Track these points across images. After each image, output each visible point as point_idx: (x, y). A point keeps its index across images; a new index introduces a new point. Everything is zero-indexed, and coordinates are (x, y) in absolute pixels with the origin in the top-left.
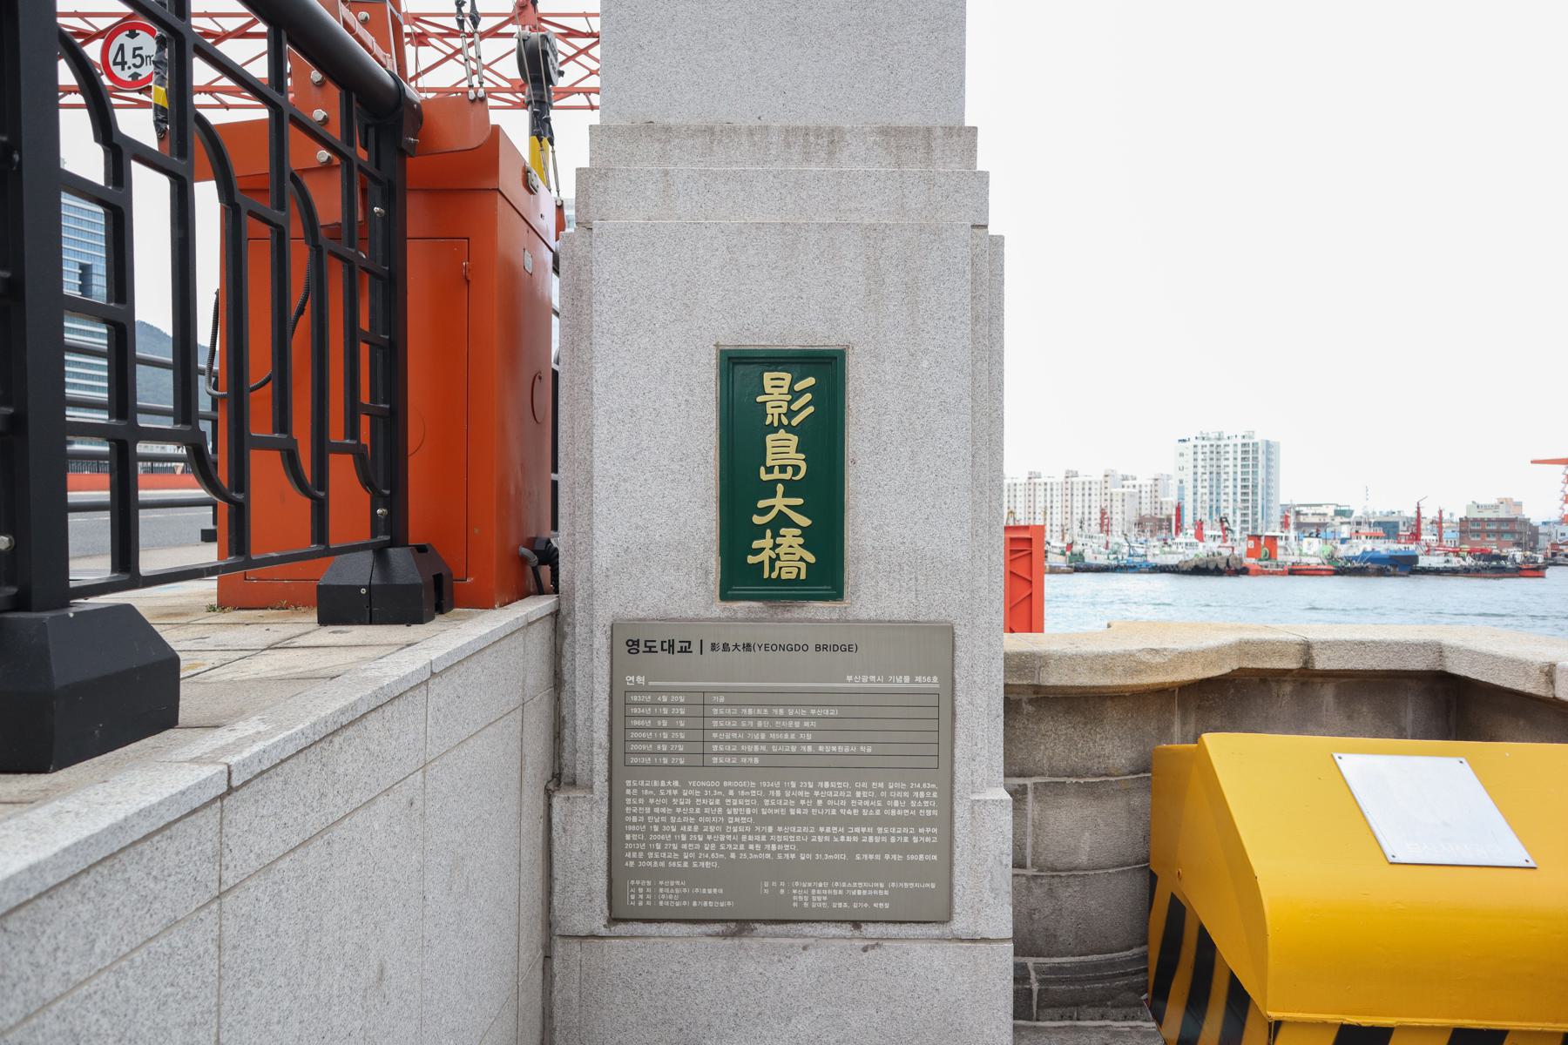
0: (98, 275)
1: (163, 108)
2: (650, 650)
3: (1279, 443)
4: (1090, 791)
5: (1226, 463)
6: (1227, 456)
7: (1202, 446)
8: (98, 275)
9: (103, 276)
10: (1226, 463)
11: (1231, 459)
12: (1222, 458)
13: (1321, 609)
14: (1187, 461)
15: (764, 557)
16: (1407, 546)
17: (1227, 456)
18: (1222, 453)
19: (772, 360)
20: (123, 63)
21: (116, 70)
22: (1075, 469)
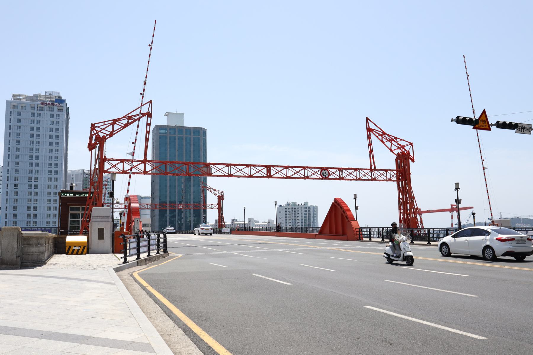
6: (298, 212)
11: (300, 214)
17: (298, 212)
18: (296, 211)
20: (323, 175)
21: (323, 176)
22: (236, 218)
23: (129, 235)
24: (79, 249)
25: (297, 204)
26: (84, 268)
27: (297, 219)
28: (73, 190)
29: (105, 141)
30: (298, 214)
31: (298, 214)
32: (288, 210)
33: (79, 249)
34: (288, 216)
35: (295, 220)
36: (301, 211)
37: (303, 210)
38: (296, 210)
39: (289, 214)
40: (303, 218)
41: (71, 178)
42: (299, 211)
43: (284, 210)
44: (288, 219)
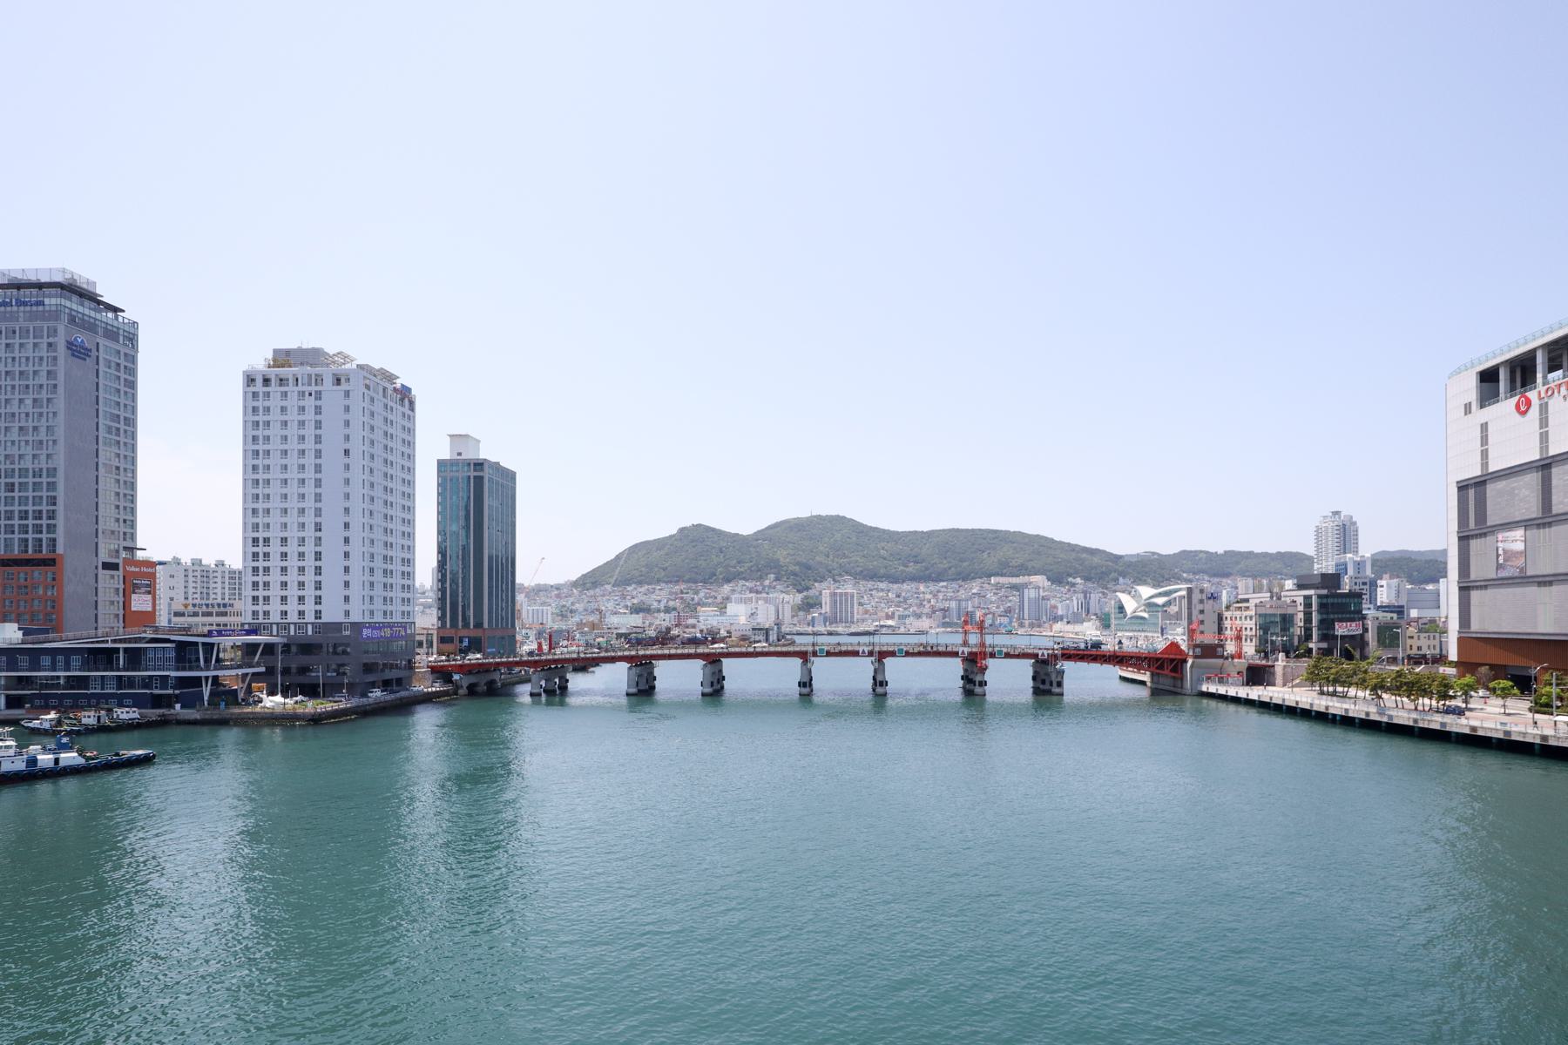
0: (1544, 438)
1: (669, 632)
2: (185, 587)
3: (244, 372)
4: (1104, 656)
5: (215, 585)
6: (215, 580)
7: (193, 571)
8: (1544, 438)
9: (1485, 464)
10: (215, 585)
11: (220, 583)
12: (211, 582)
13: (848, 634)
14: (178, 582)
15: (1046, 652)
16: (1264, 662)
17: (215, 580)
18: (211, 577)
19: (1540, 579)
23: (247, 674)
24: (1492, 667)
25: (204, 562)
26: (827, 815)
27: (211, 592)
28: (1469, 627)
29: (1216, 553)
30: (216, 583)
31: (216, 583)
32: (191, 574)
33: (1492, 667)
34: (191, 585)
35: (208, 594)
36: (223, 577)
37: (227, 575)
38: (211, 576)
39: (194, 582)
40: (227, 591)
41: (459, 457)
42: (216, 577)
43: (183, 573)
44: (191, 590)
